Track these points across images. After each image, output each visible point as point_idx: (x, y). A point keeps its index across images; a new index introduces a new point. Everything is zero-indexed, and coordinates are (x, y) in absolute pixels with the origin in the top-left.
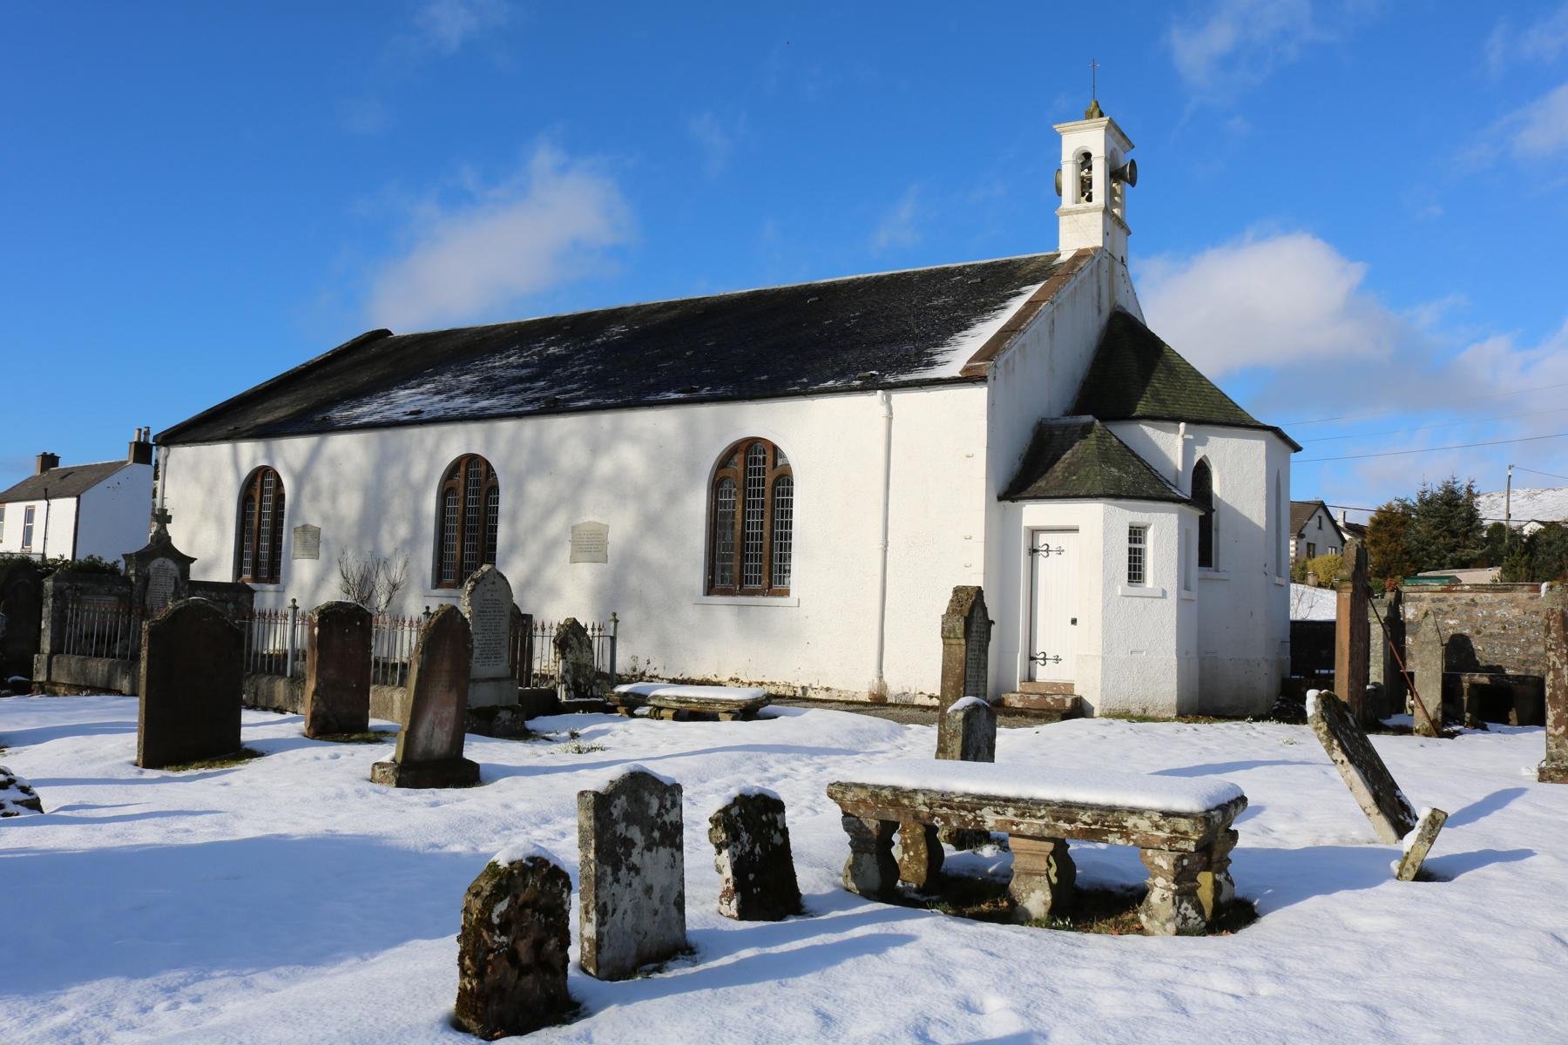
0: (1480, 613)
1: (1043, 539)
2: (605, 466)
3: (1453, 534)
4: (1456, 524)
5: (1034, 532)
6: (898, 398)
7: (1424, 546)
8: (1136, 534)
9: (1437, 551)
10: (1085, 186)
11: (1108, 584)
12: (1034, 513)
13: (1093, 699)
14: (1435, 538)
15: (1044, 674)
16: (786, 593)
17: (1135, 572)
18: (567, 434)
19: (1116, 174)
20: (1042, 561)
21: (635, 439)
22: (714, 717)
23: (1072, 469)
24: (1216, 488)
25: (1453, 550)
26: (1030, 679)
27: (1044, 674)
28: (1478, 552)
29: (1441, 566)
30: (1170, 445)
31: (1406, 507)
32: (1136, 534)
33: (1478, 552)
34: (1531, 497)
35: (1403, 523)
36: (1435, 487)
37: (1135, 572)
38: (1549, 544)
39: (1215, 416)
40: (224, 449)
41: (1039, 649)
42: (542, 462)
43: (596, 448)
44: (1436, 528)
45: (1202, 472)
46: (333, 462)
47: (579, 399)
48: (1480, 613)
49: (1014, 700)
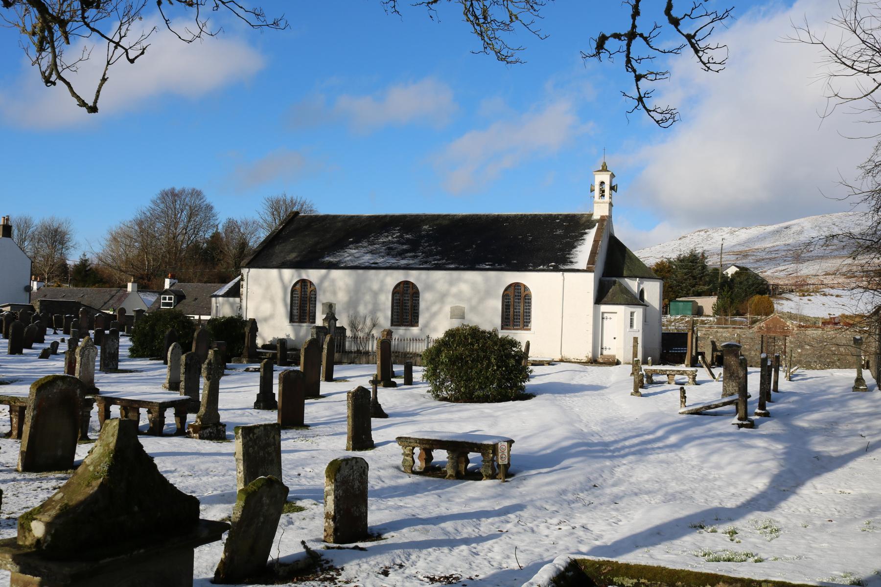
0: (719, 335)
1: (605, 315)
2: (454, 290)
3: (694, 278)
4: (696, 272)
5: (603, 313)
6: (566, 274)
7: (680, 282)
8: (632, 314)
9: (686, 287)
10: (602, 192)
11: (625, 328)
12: (604, 308)
13: (621, 360)
14: (685, 280)
15: (605, 353)
16: (530, 329)
17: (632, 326)
18: (439, 277)
19: (612, 188)
20: (605, 320)
21: (466, 281)
22: (543, 365)
23: (614, 295)
24: (646, 298)
25: (694, 286)
26: (602, 354)
27: (605, 353)
28: (706, 287)
29: (687, 295)
30: (633, 285)
31: (670, 262)
32: (632, 314)
33: (706, 287)
34: (732, 233)
35: (669, 271)
36: (685, 251)
37: (632, 326)
38: (741, 283)
39: (646, 275)
40: (274, 272)
41: (604, 346)
42: (429, 287)
43: (451, 283)
44: (686, 274)
45: (642, 292)
46: (333, 281)
47: (449, 264)
48: (719, 335)
49: (601, 360)
